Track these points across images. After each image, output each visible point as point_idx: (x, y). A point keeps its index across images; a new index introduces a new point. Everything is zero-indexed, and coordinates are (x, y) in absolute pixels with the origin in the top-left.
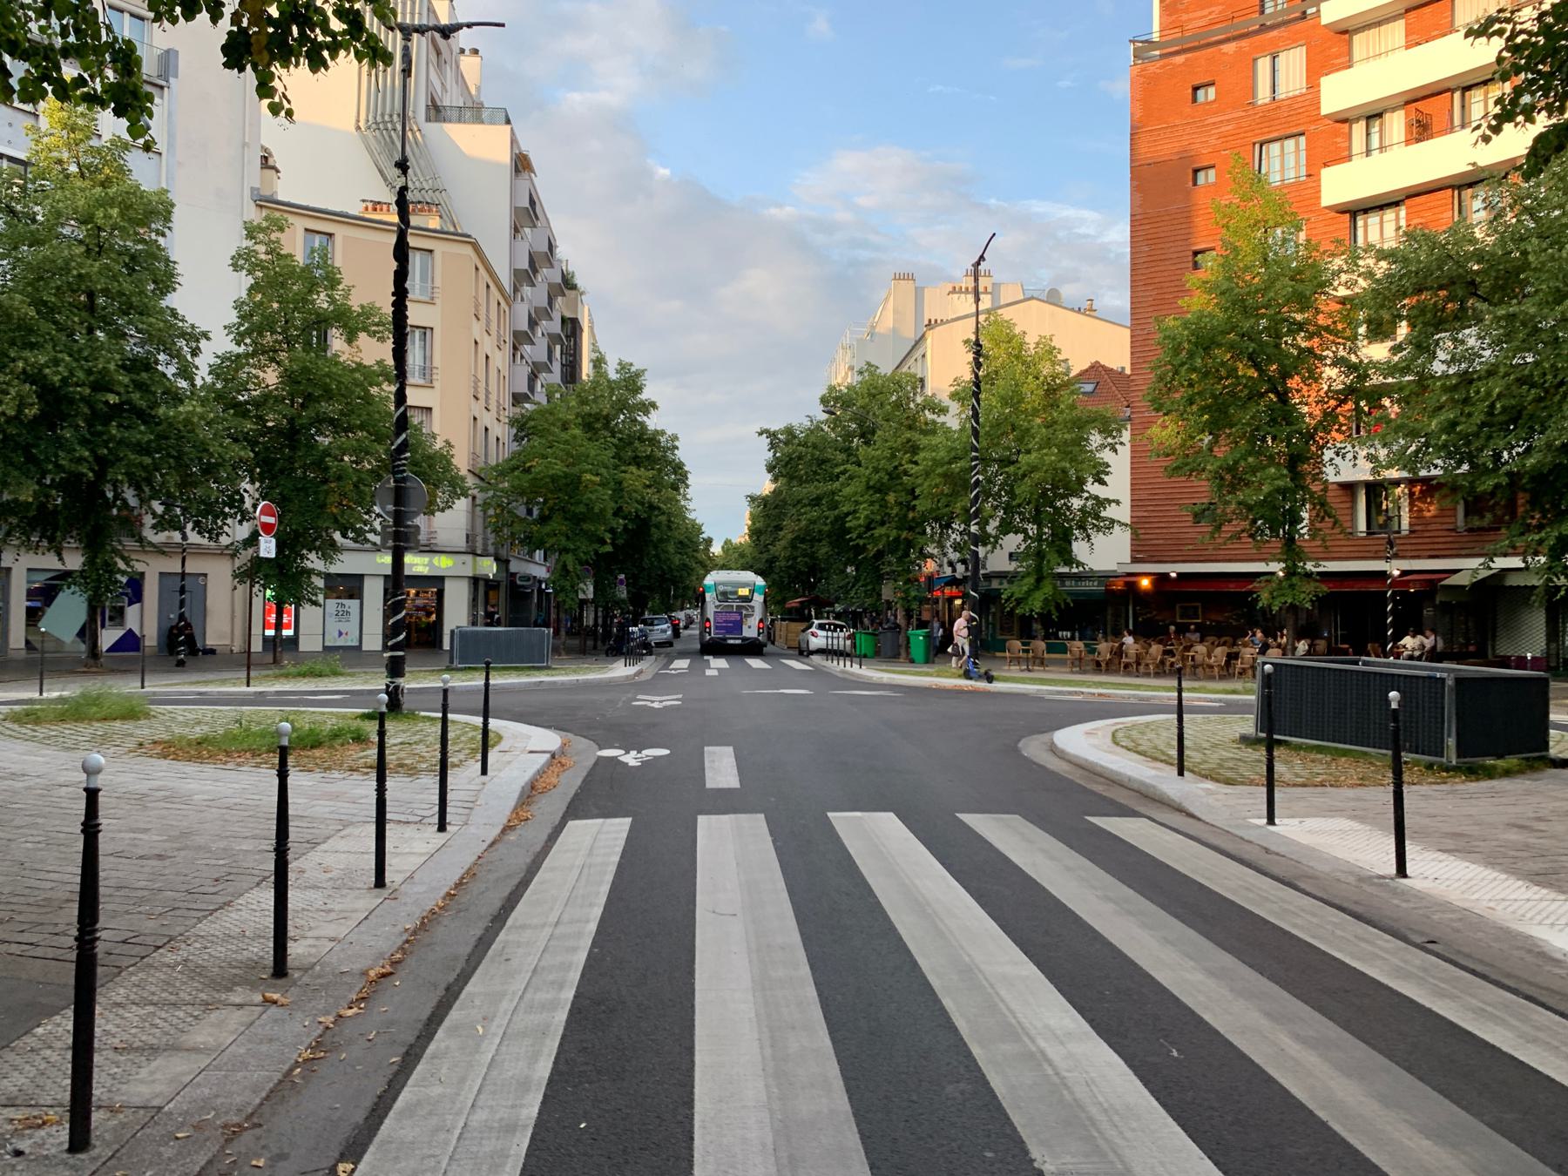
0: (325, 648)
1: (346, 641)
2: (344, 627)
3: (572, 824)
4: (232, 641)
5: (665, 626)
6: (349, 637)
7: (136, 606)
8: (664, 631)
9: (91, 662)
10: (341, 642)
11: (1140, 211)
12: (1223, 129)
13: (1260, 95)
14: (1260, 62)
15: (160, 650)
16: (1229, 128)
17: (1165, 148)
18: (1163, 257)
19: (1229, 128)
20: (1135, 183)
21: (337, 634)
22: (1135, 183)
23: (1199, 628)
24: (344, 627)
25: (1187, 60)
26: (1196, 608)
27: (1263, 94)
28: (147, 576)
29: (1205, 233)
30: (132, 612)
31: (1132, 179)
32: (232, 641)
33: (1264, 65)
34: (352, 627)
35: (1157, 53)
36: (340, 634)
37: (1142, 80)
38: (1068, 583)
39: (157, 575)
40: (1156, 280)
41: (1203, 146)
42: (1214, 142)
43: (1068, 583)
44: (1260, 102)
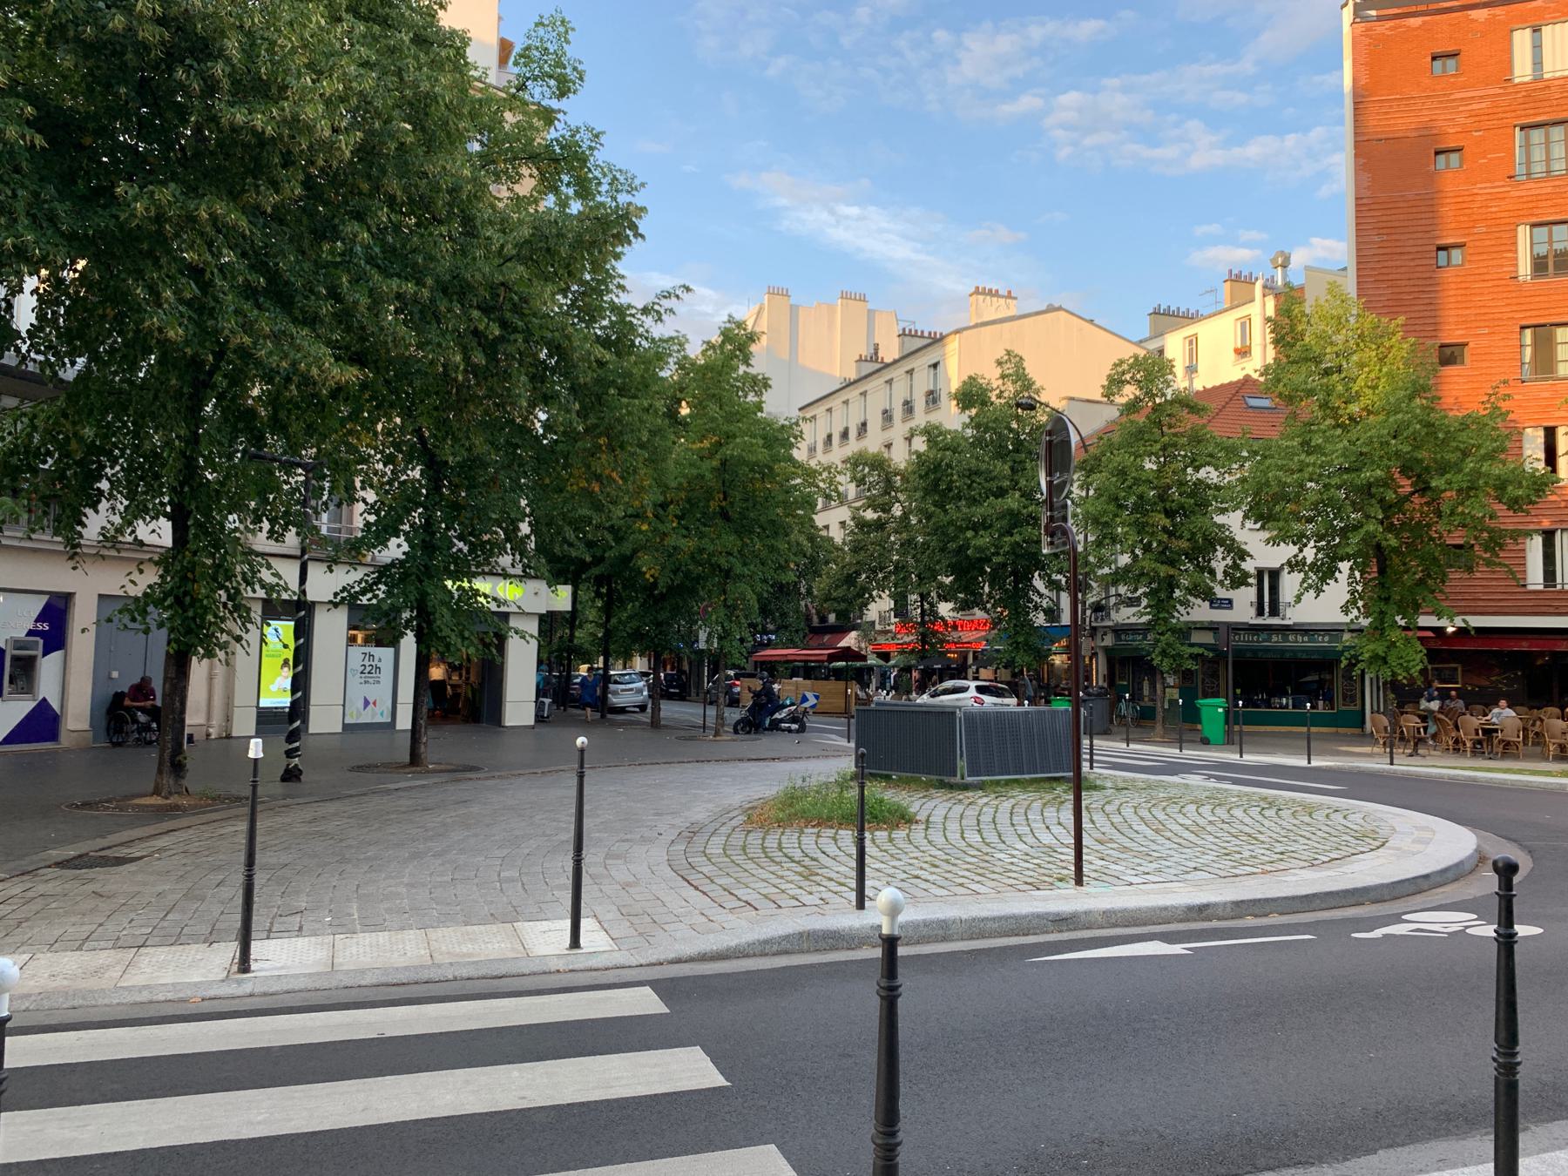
0: (346, 727)
1: (373, 716)
2: (372, 692)
3: (647, 990)
4: (209, 718)
5: (641, 684)
6: (378, 709)
7: (56, 656)
8: (640, 691)
9: (168, 781)
10: (366, 717)
11: (1368, 194)
12: (1475, 107)
13: (1517, 71)
14: (1517, 35)
15: (95, 739)
16: (1484, 105)
17: (1402, 122)
18: (1398, 250)
19: (1484, 105)
20: (1362, 161)
21: (361, 704)
22: (1362, 161)
23: (1461, 694)
24: (372, 692)
25: (1424, 23)
26: (1456, 669)
27: (1522, 70)
28: (78, 600)
29: (1453, 225)
30: (48, 667)
31: (1356, 156)
32: (209, 718)
33: (1522, 40)
34: (382, 692)
35: (1373, 13)
36: (366, 703)
37: (1368, 41)
38: (1274, 638)
39: (96, 598)
40: (1390, 277)
41: (1452, 127)
42: (1462, 121)
43: (1274, 638)
44: (1517, 81)
